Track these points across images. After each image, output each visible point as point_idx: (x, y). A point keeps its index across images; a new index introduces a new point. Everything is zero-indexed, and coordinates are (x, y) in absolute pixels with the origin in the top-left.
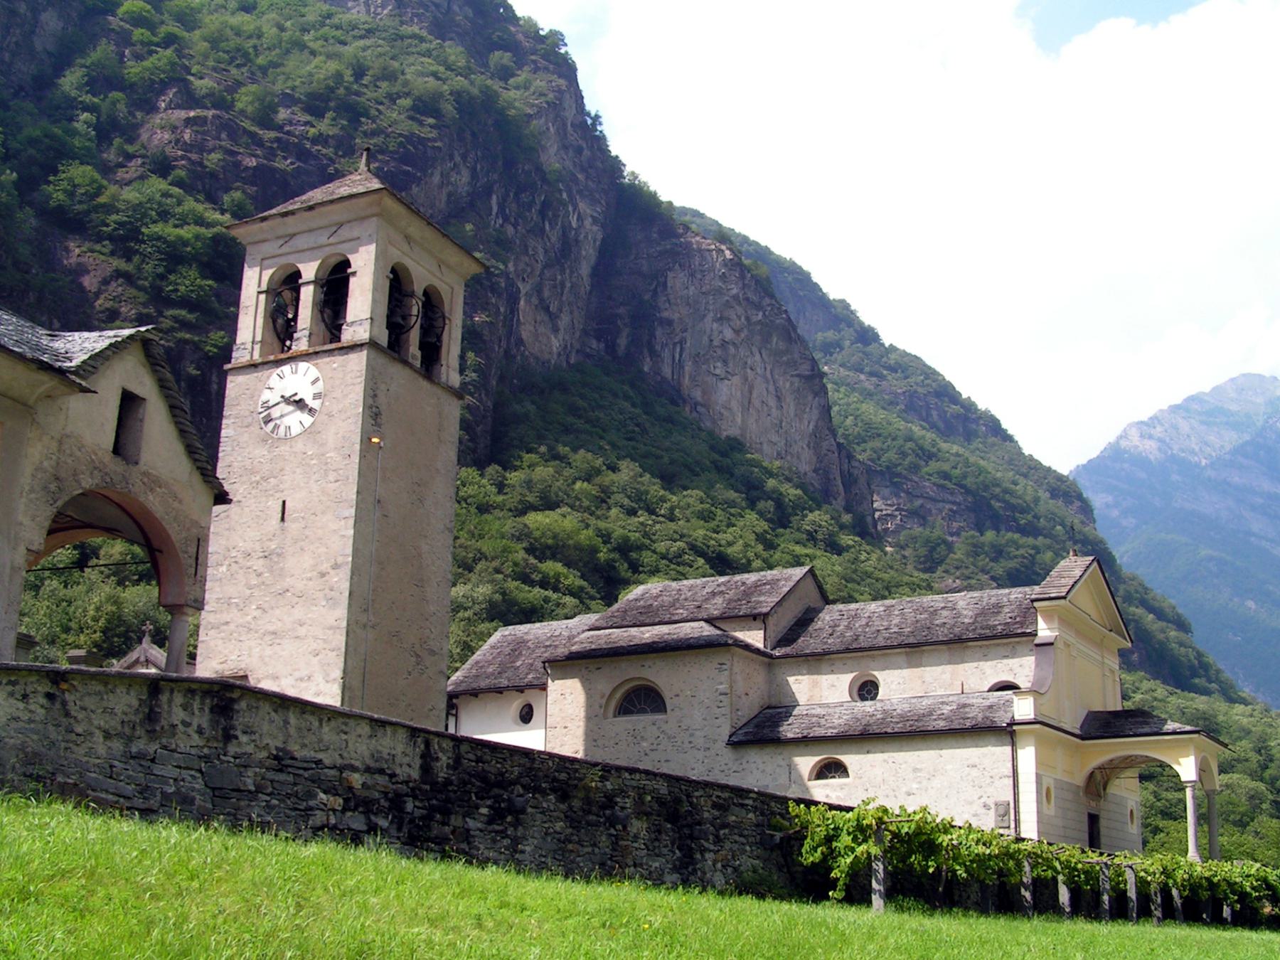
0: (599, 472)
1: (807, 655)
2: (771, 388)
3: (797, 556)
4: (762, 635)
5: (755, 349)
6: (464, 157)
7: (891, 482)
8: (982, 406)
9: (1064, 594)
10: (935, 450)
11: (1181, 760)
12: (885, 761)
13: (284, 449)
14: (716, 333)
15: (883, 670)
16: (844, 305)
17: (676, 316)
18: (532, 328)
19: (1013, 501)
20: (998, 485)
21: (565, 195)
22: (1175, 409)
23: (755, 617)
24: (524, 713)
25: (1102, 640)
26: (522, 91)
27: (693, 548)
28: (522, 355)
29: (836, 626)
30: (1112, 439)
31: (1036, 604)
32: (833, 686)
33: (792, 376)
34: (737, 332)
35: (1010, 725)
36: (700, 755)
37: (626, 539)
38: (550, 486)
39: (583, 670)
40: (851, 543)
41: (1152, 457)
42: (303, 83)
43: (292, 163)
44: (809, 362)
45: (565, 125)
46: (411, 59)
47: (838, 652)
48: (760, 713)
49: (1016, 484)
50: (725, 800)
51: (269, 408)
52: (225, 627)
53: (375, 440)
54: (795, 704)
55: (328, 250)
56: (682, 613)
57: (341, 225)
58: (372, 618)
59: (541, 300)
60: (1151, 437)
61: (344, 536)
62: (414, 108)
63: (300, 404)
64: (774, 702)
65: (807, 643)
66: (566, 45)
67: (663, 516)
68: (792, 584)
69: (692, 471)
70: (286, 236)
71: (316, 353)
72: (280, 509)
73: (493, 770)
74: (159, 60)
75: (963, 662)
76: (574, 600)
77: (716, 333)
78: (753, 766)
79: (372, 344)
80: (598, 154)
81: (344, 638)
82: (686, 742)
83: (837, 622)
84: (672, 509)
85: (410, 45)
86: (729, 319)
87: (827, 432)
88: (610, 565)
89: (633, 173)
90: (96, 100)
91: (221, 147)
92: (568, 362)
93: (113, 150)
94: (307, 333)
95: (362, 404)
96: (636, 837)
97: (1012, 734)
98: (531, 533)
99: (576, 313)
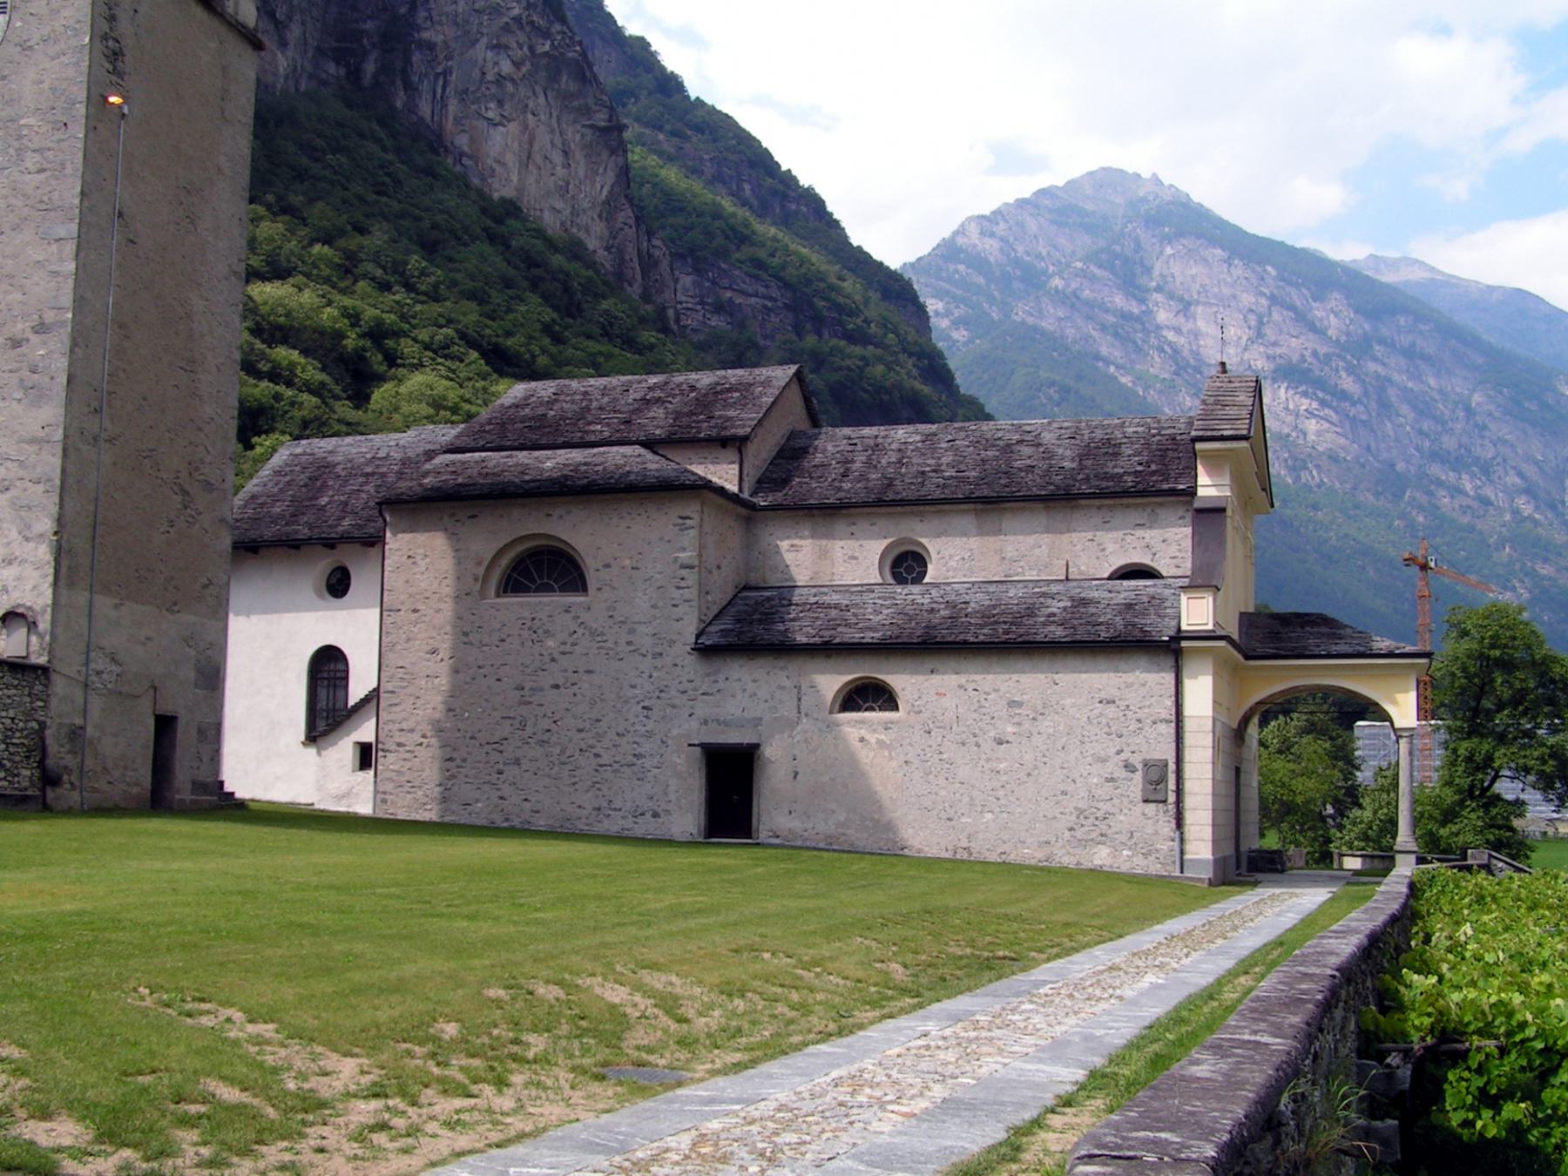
1: (811, 508)
2: (558, 141)
4: (736, 472)
5: (538, 89)
7: (694, 269)
8: (804, 181)
10: (746, 232)
11: (1399, 697)
12: (960, 687)
14: (490, 65)
15: (938, 536)
16: (642, 43)
17: (439, 39)
19: (841, 300)
20: (822, 280)
22: (1022, 203)
24: (334, 581)
27: (463, 336)
30: (947, 234)
31: (1199, 446)
33: (584, 126)
34: (517, 65)
36: (646, 664)
37: (379, 323)
38: (280, 248)
39: (446, 519)
40: (653, 340)
41: (992, 260)
44: (605, 110)
47: (865, 505)
48: (735, 596)
53: (114, 99)
58: (107, 424)
60: (992, 235)
61: (56, 273)
64: (754, 579)
67: (424, 293)
68: (777, 392)
76: (314, 399)
77: (490, 65)
78: (736, 685)
82: (622, 642)
84: (436, 286)
86: (507, 47)
87: (624, 201)
88: (359, 355)
92: (297, 90)
95: (88, 29)
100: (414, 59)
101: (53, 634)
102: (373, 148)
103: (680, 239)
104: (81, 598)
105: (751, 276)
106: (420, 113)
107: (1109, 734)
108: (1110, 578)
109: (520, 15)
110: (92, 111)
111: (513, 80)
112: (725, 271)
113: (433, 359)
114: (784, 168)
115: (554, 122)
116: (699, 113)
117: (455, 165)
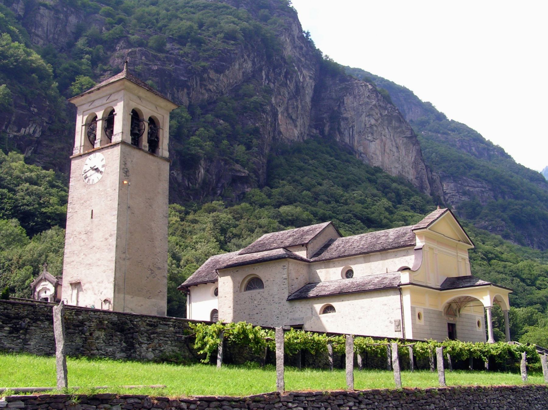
0: (314, 186)
1: (323, 260)
2: (394, 144)
3: (404, 216)
5: (385, 127)
6: (248, 56)
8: (495, 143)
9: (425, 226)
10: (473, 165)
11: (484, 297)
13: (92, 188)
14: (367, 122)
16: (429, 104)
18: (285, 127)
21: (296, 68)
23: (303, 245)
25: (457, 246)
26: (274, 25)
27: (355, 216)
28: (282, 139)
29: (339, 246)
32: (335, 273)
33: (403, 137)
35: (399, 286)
36: (277, 306)
42: (176, 32)
43: (173, 66)
45: (294, 38)
46: (223, 17)
47: (336, 258)
49: (512, 177)
50: (154, 322)
51: (86, 172)
52: (72, 263)
53: (125, 182)
54: (320, 281)
55: (106, 106)
56: (275, 245)
57: (111, 95)
58: (128, 256)
59: (288, 114)
61: (113, 223)
62: (225, 37)
63: (97, 170)
64: (311, 281)
65: (326, 255)
66: (292, 3)
69: (358, 183)
70: (91, 101)
71: (102, 148)
72: (91, 213)
73: (13, 312)
74: (116, 29)
75: (387, 259)
77: (367, 122)
79: (123, 143)
80: (310, 49)
81: (114, 265)
82: (271, 300)
83: (340, 245)
85: (222, 11)
86: (372, 115)
87: (421, 161)
89: (326, 56)
90: (91, 49)
91: (142, 62)
93: (98, 69)
94: (99, 140)
95: (119, 168)
96: (98, 338)
97: (400, 290)
98: (281, 215)
99: (305, 118)
100: (341, 124)
101: (114, 304)
102: (327, 156)
103: (447, 171)
104: (122, 296)
105: (475, 180)
106: (345, 141)
107: (385, 314)
108: (398, 271)
109: (376, 104)
110: (120, 186)
111: (376, 126)
112: (465, 180)
113: (344, 225)
114: (487, 140)
115: (392, 137)
116: (453, 125)
117: (359, 157)
